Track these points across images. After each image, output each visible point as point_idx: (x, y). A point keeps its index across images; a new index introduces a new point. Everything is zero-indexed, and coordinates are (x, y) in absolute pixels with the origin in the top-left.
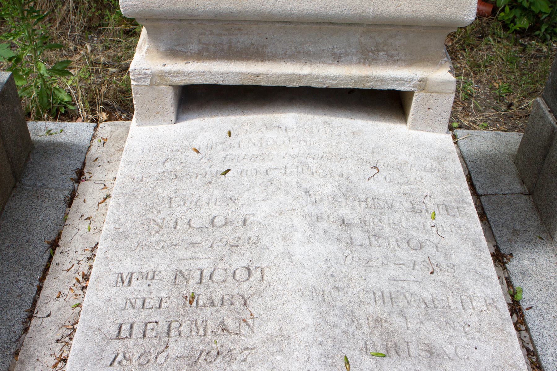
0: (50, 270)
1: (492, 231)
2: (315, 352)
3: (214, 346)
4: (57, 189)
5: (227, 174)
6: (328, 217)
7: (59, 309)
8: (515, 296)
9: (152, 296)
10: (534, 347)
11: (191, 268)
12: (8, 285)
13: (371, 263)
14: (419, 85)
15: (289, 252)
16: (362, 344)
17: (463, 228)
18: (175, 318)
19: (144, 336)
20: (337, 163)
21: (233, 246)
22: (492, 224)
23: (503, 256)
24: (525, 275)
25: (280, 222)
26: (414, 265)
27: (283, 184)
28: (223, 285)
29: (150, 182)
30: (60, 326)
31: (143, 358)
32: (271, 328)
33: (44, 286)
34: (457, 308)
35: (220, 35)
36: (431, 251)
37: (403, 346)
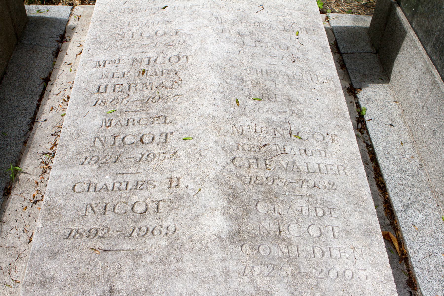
0: (45, 95)
1: (349, 75)
2: (218, 96)
3: (157, 94)
5: (165, 9)
6: (229, 31)
7: (53, 117)
8: (361, 112)
9: (118, 71)
10: (371, 142)
11: (142, 57)
12: (17, 103)
13: (255, 55)
15: (204, 48)
16: (247, 94)
17: (316, 41)
18: (133, 82)
19: (114, 91)
20: (236, 3)
21: (169, 45)
22: (349, 71)
23: (355, 89)
24: (369, 101)
25: (199, 33)
26: (283, 57)
27: (202, 13)
28: (162, 65)
29: (115, 14)
30: (54, 126)
31: (114, 102)
32: (192, 85)
33: (41, 104)
34: (308, 80)
36: (294, 51)
37: (271, 95)
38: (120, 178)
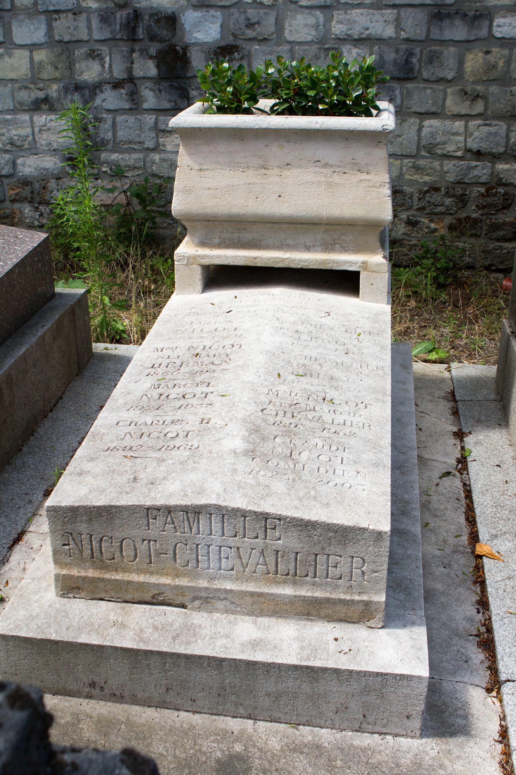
4: (109, 380)
10: (470, 482)
14: (363, 266)
29: (180, 317)
32: (240, 363)
35: (233, 233)
38: (158, 418)
